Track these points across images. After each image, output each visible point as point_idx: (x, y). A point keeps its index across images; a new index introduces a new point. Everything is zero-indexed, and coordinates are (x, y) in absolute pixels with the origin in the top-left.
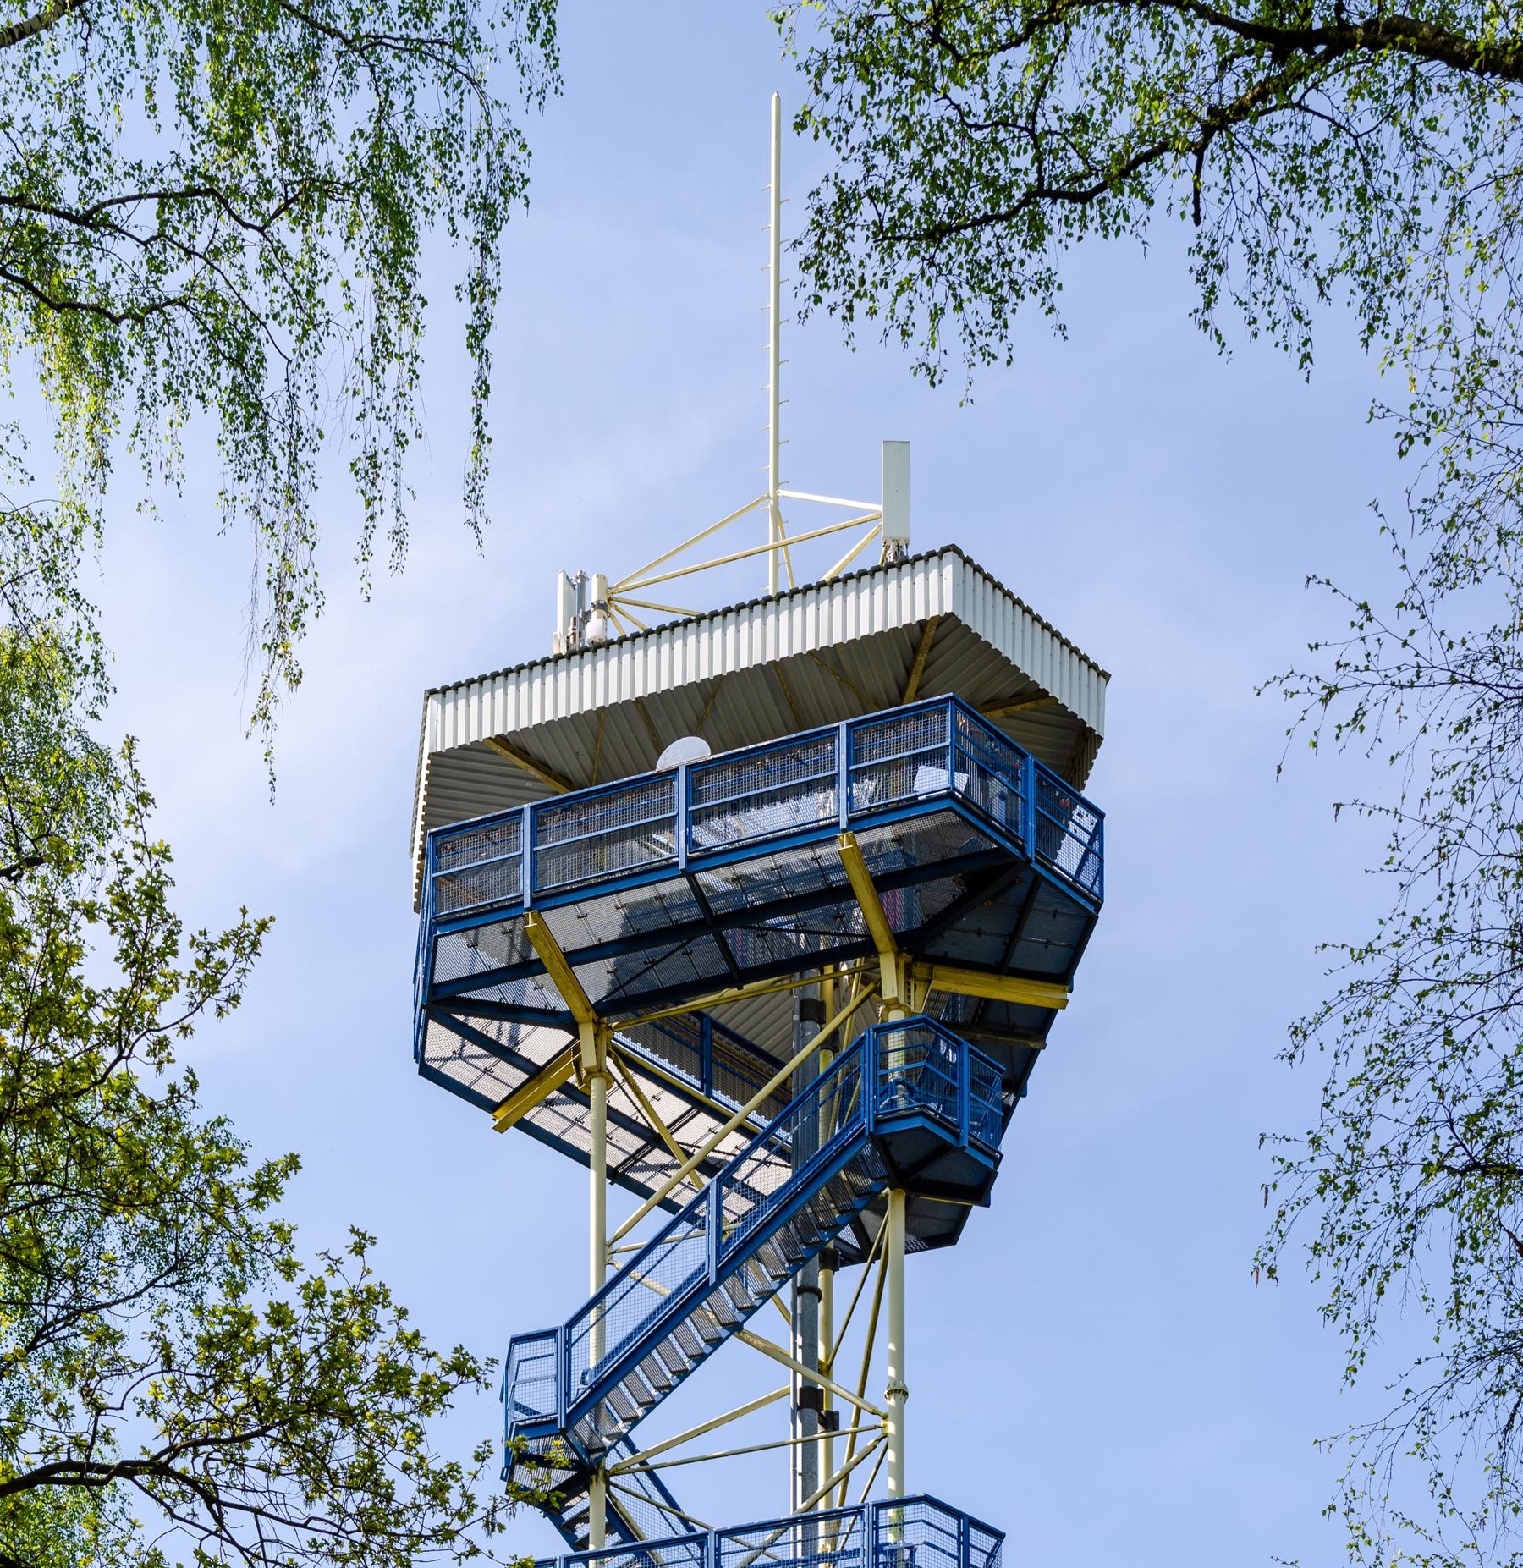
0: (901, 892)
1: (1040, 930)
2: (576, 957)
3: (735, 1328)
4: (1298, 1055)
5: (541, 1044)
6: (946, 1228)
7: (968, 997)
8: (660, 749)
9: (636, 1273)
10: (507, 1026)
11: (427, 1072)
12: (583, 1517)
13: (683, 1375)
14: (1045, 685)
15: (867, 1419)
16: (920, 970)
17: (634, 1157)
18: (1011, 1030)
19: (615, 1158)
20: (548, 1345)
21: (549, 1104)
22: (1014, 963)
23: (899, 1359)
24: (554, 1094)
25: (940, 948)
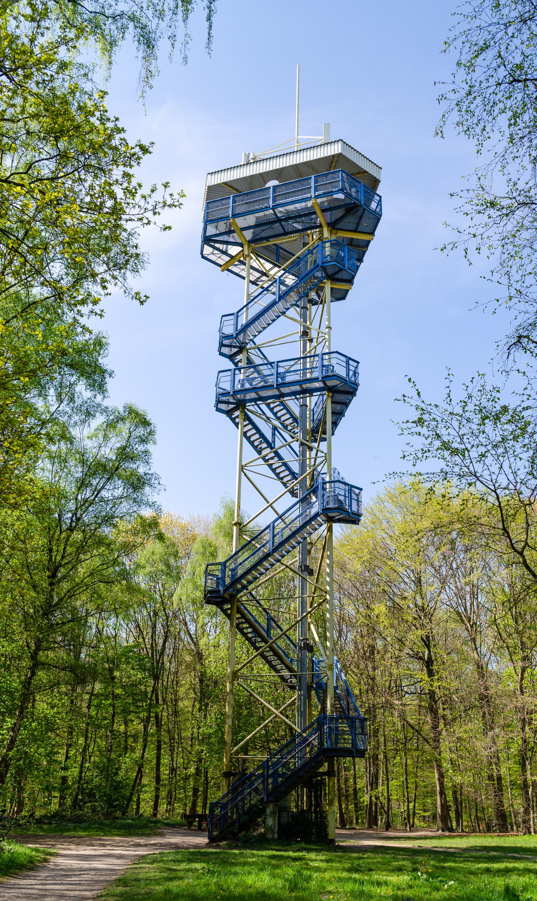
0: (329, 213)
1: (365, 224)
2: (243, 229)
3: (283, 313)
4: (448, 50)
5: (234, 250)
6: (343, 296)
7: (347, 238)
8: (266, 183)
9: (255, 300)
10: (225, 246)
11: (203, 257)
12: (240, 361)
13: (269, 325)
14: (365, 169)
15: (320, 335)
16: (334, 231)
17: (258, 278)
18: (358, 246)
19: (253, 278)
20: (232, 317)
21: (236, 265)
22: (359, 230)
23: (329, 320)
24: (237, 263)
25: (339, 226)
